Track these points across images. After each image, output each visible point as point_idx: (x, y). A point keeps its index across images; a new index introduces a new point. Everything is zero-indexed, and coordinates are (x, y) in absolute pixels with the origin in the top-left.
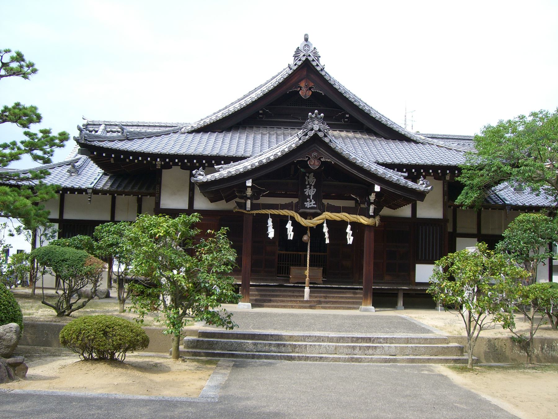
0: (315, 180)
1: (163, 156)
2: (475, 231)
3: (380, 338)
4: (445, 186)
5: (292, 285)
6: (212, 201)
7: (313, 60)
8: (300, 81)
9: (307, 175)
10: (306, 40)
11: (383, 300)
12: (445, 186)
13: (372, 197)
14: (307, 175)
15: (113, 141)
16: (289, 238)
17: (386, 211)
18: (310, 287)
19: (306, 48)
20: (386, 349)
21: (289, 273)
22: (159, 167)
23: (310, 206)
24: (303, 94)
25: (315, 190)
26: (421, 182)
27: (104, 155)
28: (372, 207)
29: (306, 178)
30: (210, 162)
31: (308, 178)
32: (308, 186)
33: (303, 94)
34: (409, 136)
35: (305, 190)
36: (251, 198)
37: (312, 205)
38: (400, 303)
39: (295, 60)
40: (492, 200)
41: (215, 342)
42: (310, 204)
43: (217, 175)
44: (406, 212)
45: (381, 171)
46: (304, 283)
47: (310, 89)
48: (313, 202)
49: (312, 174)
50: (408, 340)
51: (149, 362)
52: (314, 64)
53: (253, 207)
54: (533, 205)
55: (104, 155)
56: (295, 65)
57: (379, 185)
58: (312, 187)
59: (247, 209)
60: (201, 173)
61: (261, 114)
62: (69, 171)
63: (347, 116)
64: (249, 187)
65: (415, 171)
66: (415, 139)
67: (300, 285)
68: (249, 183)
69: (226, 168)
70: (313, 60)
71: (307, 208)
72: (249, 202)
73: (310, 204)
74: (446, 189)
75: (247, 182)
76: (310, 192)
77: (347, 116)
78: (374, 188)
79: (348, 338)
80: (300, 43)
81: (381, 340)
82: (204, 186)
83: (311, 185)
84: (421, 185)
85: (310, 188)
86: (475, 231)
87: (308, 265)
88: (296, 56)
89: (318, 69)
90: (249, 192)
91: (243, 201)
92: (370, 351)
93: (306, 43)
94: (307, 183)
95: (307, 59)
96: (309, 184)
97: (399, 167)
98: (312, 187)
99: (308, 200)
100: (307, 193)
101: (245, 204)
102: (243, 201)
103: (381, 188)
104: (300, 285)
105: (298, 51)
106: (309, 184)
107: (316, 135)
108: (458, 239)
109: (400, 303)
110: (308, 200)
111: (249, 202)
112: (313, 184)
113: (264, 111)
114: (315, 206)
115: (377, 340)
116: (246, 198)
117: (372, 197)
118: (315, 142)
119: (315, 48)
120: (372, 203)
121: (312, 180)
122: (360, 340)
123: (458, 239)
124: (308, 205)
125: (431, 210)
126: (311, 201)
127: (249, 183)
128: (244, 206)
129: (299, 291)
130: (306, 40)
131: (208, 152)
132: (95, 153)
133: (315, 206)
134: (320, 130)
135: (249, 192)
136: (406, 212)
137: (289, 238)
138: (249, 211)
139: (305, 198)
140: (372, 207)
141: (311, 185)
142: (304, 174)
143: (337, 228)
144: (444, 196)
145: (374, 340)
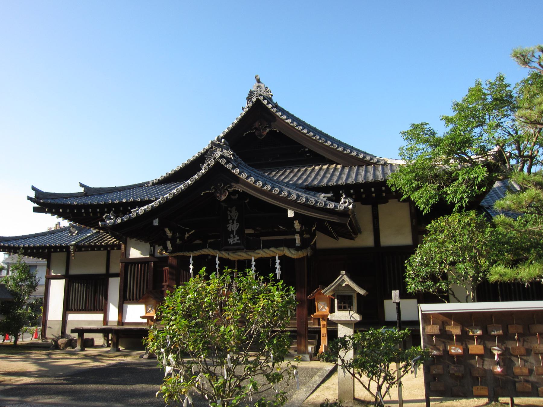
0: (238, 214)
9: (229, 209)
10: (259, 81)
14: (229, 209)
16: (397, 291)
19: (259, 89)
23: (234, 242)
25: (238, 224)
26: (343, 201)
29: (228, 212)
31: (231, 212)
32: (231, 221)
33: (264, 134)
35: (228, 226)
37: (236, 241)
42: (233, 240)
48: (237, 238)
51: (50, 398)
58: (235, 222)
71: (230, 245)
75: (154, 221)
76: (233, 227)
85: (233, 223)
88: (249, 99)
93: (258, 84)
94: (229, 218)
97: (336, 192)
98: (235, 222)
99: (232, 236)
100: (229, 229)
103: (295, 212)
105: (251, 93)
106: (231, 219)
107: (217, 163)
110: (232, 236)
112: (236, 219)
114: (239, 242)
124: (231, 241)
126: (234, 237)
130: (259, 81)
133: (239, 242)
137: (397, 291)
139: (229, 234)
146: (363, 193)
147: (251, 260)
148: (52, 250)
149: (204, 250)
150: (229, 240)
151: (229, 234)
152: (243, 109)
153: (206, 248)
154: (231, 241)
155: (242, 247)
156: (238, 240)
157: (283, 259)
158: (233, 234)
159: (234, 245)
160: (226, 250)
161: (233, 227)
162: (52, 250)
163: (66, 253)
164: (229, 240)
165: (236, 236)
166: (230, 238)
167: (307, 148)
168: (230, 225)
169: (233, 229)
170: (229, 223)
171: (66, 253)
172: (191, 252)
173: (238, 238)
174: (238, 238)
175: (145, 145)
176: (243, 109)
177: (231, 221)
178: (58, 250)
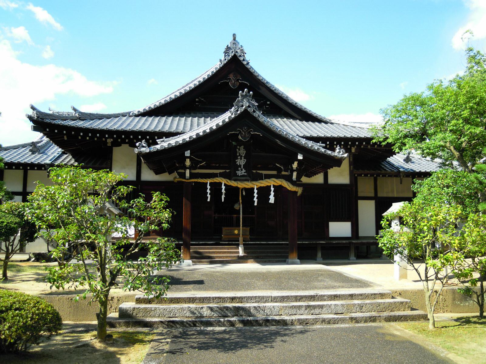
0: (245, 152)
1: (111, 133)
2: (372, 195)
3: (324, 296)
4: (351, 157)
5: (227, 243)
6: (157, 173)
7: (240, 56)
8: (229, 74)
9: (238, 147)
10: (234, 39)
11: (306, 255)
12: (351, 157)
13: (295, 165)
14: (238, 147)
15: (65, 120)
17: (305, 180)
18: (244, 244)
20: (333, 307)
21: (221, 232)
22: (109, 145)
23: (241, 174)
24: (233, 80)
25: (245, 160)
27: (56, 131)
28: (295, 174)
29: (237, 150)
30: (152, 137)
31: (239, 150)
32: (239, 157)
34: (319, 118)
35: (236, 161)
36: (190, 168)
37: (243, 174)
38: (319, 255)
39: (225, 56)
40: (388, 168)
41: (153, 309)
42: (241, 172)
43: (158, 147)
44: (318, 179)
45: (303, 141)
46: (238, 241)
47: (238, 80)
48: (244, 171)
49: (243, 147)
50: (352, 296)
52: (241, 59)
53: (192, 176)
54: (422, 171)
55: (56, 131)
56: (225, 60)
57: (301, 153)
58: (243, 158)
59: (186, 178)
60: (144, 145)
61: (197, 102)
62: (30, 151)
63: (268, 103)
64: (188, 157)
65: (331, 142)
66: (325, 120)
67: (233, 243)
68: (188, 153)
69: (167, 141)
70: (240, 56)
72: (188, 172)
73: (241, 172)
74: (351, 160)
75: (186, 152)
76: (241, 162)
77: (268, 103)
78: (297, 157)
79: (292, 296)
80: (228, 41)
81: (326, 297)
82: (148, 157)
83: (242, 156)
84: (339, 152)
85: (241, 159)
86: (372, 195)
87: (241, 225)
88: (226, 52)
89: (245, 63)
90: (188, 163)
91: (183, 171)
92: (317, 311)
94: (238, 154)
95: (235, 55)
96: (240, 155)
97: (316, 139)
98: (243, 158)
99: (240, 169)
100: (238, 163)
101: (185, 173)
102: (183, 171)
104: (233, 243)
105: (228, 48)
107: (246, 110)
108: (360, 202)
109: (319, 255)
110: (240, 169)
111: (188, 172)
113: (199, 99)
115: (321, 298)
116: (185, 168)
117: (295, 165)
118: (245, 117)
119: (241, 46)
120: (295, 171)
121: (242, 151)
122: (304, 299)
123: (360, 202)
124: (239, 173)
125: (339, 176)
126: (242, 170)
127: (188, 153)
128: (183, 175)
129: (235, 248)
130: (234, 39)
131: (152, 128)
132: (48, 130)
134: (249, 107)
135: (188, 163)
136: (318, 179)
138: (187, 179)
139: (237, 167)
140: (295, 174)
141: (242, 156)
142: (235, 147)
143: (264, 192)
144: (350, 165)
145: (318, 298)
146: (349, 145)
147: (254, 188)
148: (29, 168)
149: (217, 178)
150: (237, 172)
151: (237, 167)
152: (221, 61)
153: (218, 177)
154: (239, 173)
155: (248, 178)
156: (244, 172)
157: (279, 189)
158: (241, 168)
159: (241, 176)
160: (235, 180)
161: (241, 162)
162: (29, 168)
163: (23, 171)
164: (237, 172)
165: (243, 169)
166: (238, 170)
167: (269, 101)
168: (239, 160)
169: (241, 164)
170: (237, 159)
171: (23, 171)
172: (208, 179)
173: (245, 171)
174: (245, 171)
175: (130, 82)
176: (221, 61)
177: (239, 157)
178: (14, 167)
